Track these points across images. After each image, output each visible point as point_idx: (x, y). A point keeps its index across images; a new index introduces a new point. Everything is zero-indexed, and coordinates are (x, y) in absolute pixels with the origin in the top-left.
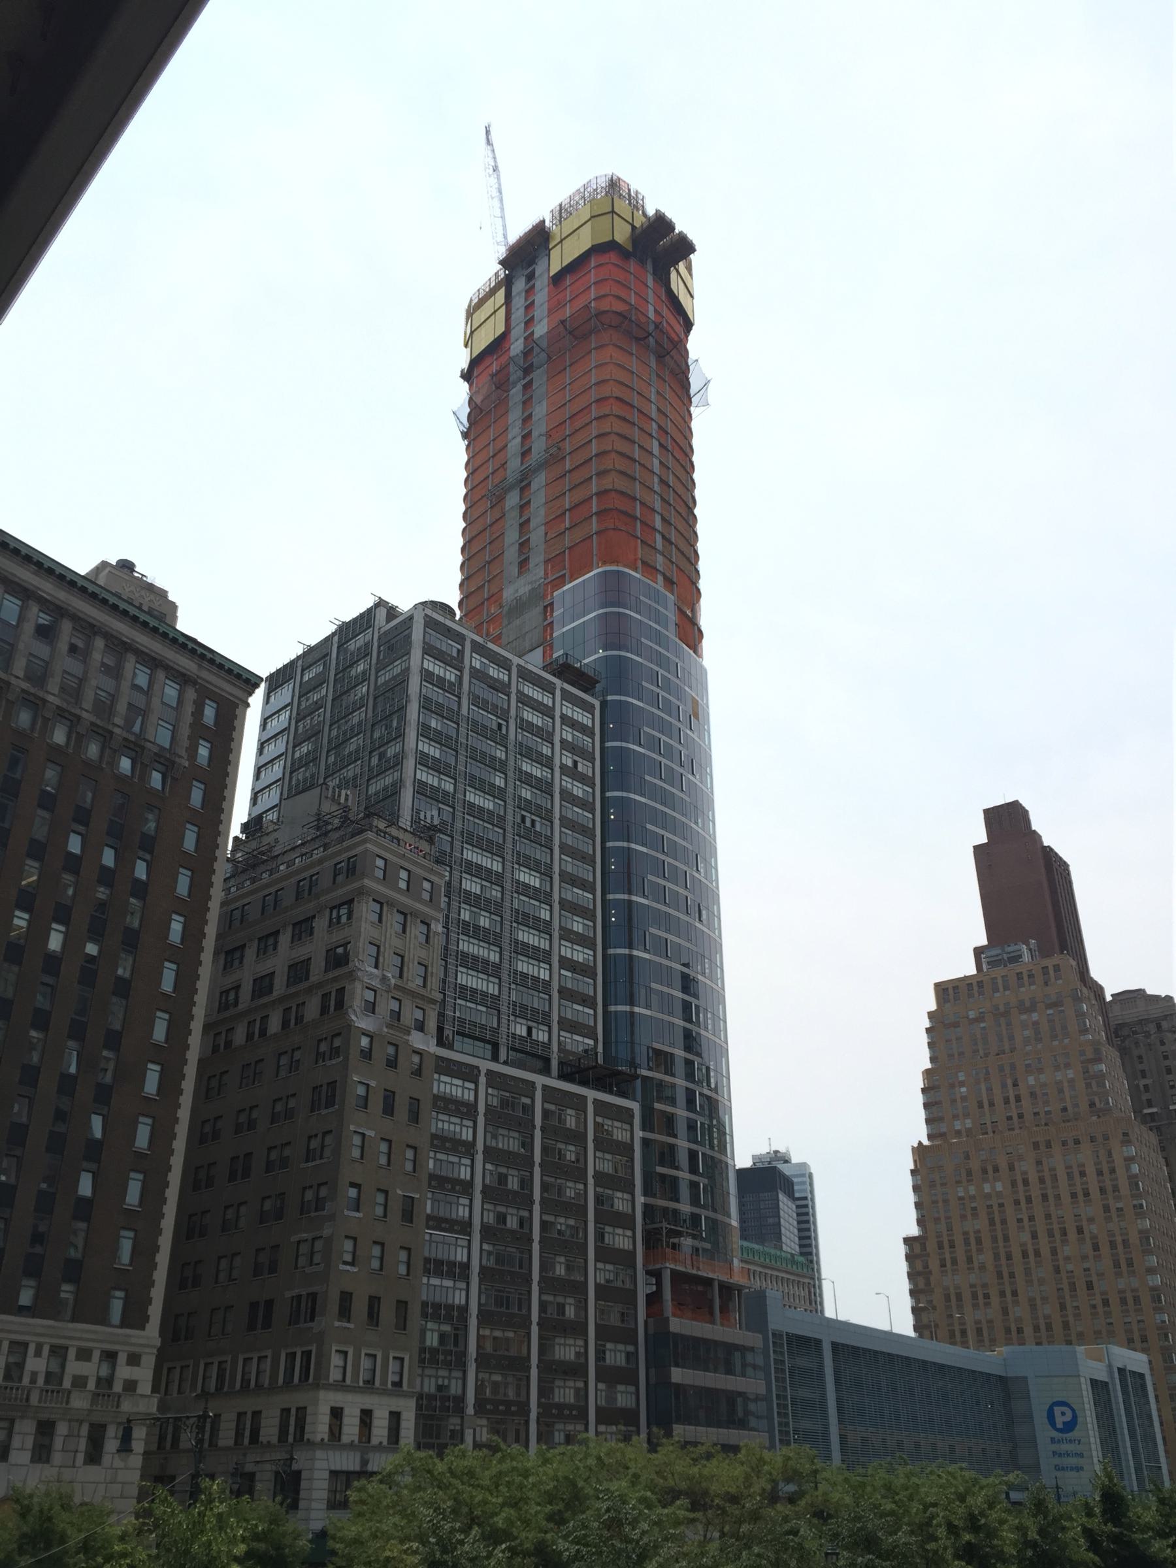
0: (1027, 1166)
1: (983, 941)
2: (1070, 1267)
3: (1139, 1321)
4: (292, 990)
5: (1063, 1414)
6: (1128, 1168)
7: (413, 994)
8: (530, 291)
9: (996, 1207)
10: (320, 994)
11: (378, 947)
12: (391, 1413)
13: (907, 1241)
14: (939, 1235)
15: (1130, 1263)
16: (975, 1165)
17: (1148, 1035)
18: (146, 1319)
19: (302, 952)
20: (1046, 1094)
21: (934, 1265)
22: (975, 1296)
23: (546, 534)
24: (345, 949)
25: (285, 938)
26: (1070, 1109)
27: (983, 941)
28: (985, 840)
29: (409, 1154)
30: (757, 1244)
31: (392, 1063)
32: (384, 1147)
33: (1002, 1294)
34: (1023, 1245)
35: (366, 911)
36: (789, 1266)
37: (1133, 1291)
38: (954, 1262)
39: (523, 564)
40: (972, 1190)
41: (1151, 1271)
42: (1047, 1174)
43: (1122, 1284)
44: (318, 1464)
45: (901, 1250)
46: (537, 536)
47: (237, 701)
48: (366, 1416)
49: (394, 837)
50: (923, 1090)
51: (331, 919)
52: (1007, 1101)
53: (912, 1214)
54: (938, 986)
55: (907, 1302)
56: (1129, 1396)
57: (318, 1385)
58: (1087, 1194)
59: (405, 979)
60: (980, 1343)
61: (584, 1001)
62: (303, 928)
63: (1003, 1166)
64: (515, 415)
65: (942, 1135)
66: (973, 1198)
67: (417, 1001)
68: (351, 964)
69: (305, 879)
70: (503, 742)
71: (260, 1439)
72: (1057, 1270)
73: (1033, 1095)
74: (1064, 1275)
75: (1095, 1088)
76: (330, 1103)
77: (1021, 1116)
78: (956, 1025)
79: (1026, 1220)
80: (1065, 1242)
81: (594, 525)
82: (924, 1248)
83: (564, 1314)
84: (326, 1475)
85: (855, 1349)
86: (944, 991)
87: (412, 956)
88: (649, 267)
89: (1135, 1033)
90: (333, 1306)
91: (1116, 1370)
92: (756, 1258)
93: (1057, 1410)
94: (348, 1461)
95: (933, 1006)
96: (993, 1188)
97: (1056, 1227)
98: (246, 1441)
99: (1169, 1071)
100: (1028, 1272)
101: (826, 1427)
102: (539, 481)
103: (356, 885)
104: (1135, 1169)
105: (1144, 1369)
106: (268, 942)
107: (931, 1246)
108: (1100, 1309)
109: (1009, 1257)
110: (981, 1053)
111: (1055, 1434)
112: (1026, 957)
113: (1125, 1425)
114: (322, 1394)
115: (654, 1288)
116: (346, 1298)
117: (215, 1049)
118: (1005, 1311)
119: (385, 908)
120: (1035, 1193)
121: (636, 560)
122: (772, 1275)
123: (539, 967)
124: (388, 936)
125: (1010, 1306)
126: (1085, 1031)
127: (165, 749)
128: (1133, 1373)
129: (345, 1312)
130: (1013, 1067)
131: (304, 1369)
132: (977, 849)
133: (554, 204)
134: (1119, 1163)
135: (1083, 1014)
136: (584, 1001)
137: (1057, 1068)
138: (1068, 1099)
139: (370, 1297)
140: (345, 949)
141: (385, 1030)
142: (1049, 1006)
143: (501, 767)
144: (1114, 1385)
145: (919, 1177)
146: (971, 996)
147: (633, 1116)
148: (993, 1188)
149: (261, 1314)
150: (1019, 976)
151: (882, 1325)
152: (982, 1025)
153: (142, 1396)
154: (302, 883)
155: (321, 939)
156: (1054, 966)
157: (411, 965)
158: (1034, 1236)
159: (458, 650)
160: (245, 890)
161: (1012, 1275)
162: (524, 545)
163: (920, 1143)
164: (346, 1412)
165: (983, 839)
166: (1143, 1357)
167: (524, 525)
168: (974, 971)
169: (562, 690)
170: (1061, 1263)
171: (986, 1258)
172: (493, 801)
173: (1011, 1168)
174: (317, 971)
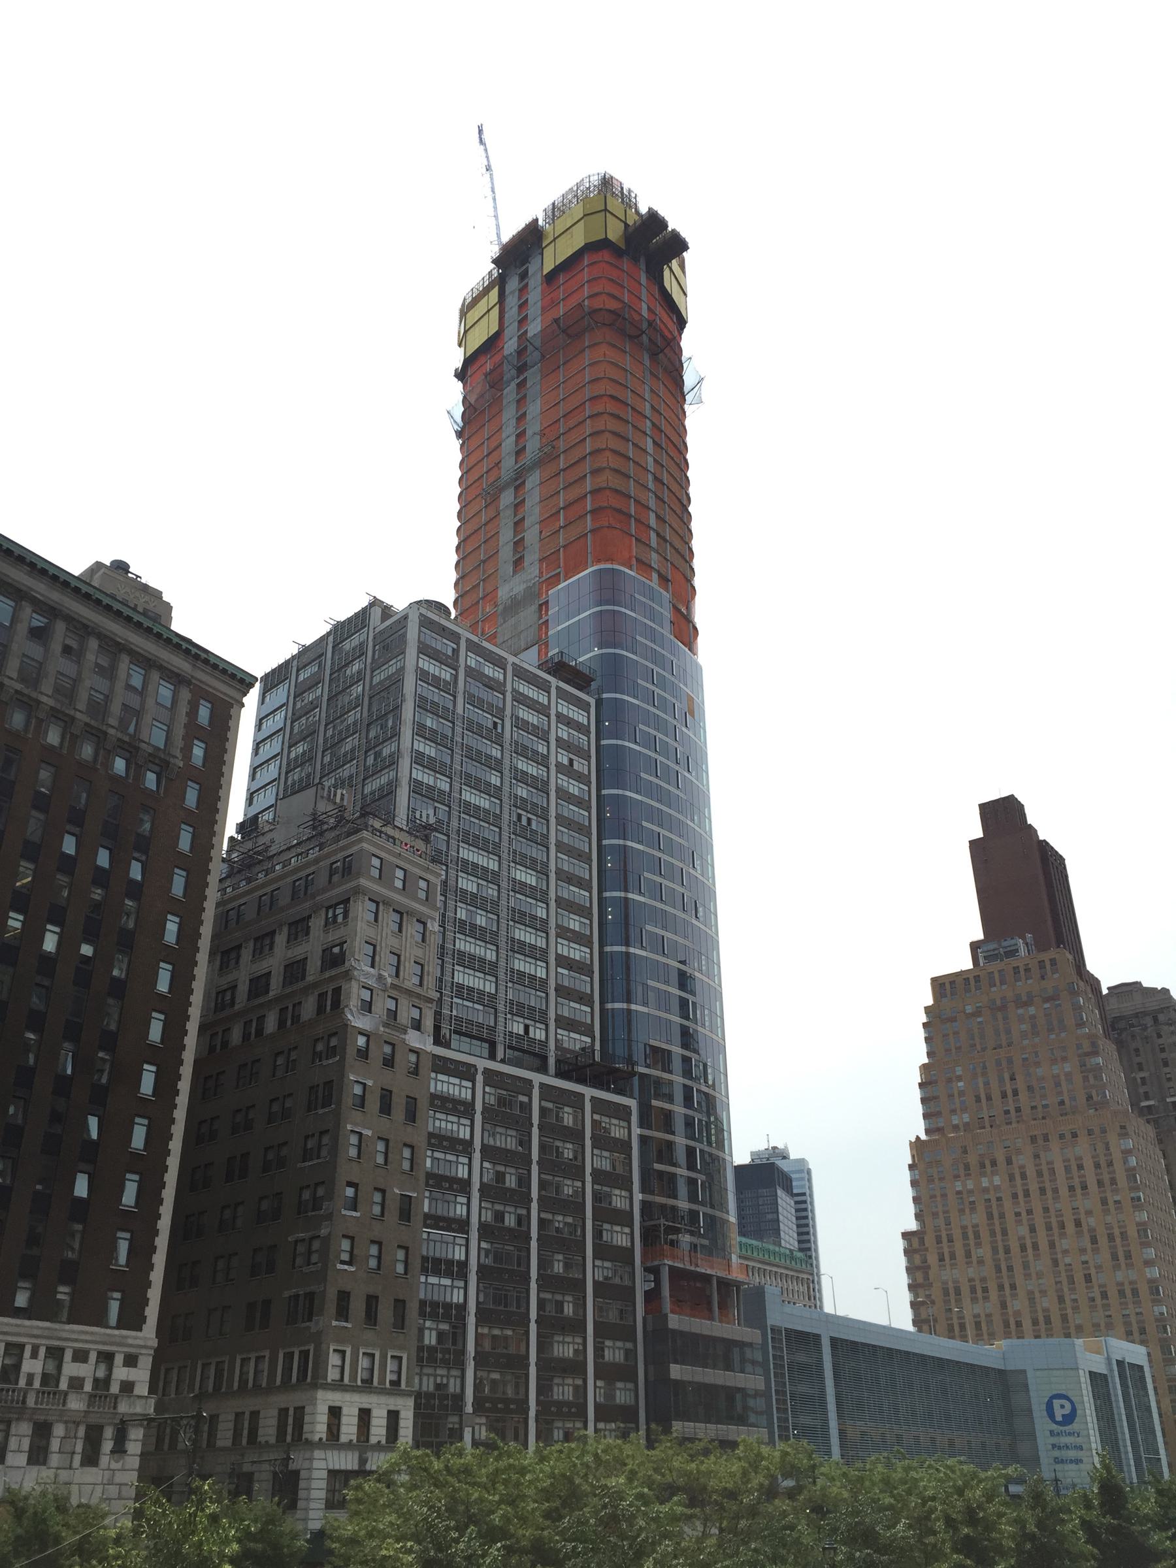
0: (1024, 1159)
1: (980, 936)
2: (1068, 1260)
3: (1137, 1314)
4: (288, 990)
5: (1062, 1407)
6: (1125, 1162)
7: (409, 993)
8: (523, 290)
9: (994, 1203)
11: (375, 946)
14: (937, 1230)
15: (1128, 1256)
21: (932, 1259)
22: (973, 1290)
23: (541, 532)
24: (341, 949)
25: (281, 939)
26: (1067, 1101)
28: (981, 835)
29: (407, 1153)
32: (381, 1146)
33: (1001, 1287)
34: (1021, 1238)
35: (362, 910)
37: (1131, 1283)
38: (953, 1256)
39: (518, 563)
40: (970, 1185)
43: (1120, 1276)
44: (316, 1464)
45: (900, 1244)
46: (531, 535)
48: (365, 1415)
49: (389, 836)
50: (920, 1085)
51: (327, 918)
52: (1004, 1095)
53: (910, 1209)
54: (934, 981)
58: (1084, 1187)
59: (401, 978)
60: (979, 1337)
61: (581, 999)
62: (299, 929)
63: (1000, 1157)
64: (509, 414)
65: (939, 1130)
66: (970, 1192)
68: (347, 964)
70: (499, 741)
72: (1055, 1263)
74: (1062, 1267)
77: (1018, 1110)
80: (1063, 1235)
83: (562, 1311)
87: (407, 954)
88: (643, 266)
89: (1132, 1026)
91: (1114, 1362)
94: (346, 1461)
95: (930, 1001)
96: (991, 1182)
100: (1026, 1266)
101: (826, 1421)
102: (533, 480)
104: (1133, 1161)
105: (1142, 1360)
106: (263, 943)
107: (930, 1240)
108: (1099, 1301)
109: (1007, 1251)
110: (979, 1047)
111: (1054, 1427)
112: (1023, 951)
114: (321, 1394)
116: (344, 1297)
117: (212, 1049)
118: (1004, 1305)
119: (381, 907)
120: (1034, 1187)
121: (630, 558)
124: (384, 935)
125: (1008, 1299)
126: (1081, 1024)
130: (1010, 1061)
132: (973, 844)
133: (547, 203)
134: (1117, 1156)
135: (1080, 1007)
136: (581, 999)
137: (1054, 1061)
140: (341, 949)
141: (382, 1029)
142: (1047, 1000)
144: (1113, 1377)
145: (917, 1172)
146: (968, 990)
147: (630, 1114)
148: (991, 1182)
150: (1016, 970)
153: (139, 1397)
154: (334, 866)
156: (1051, 960)
158: (1033, 1230)
160: (240, 891)
161: (1010, 1268)
162: (519, 544)
163: (918, 1138)
165: (979, 833)
166: (1142, 1350)
167: (518, 524)
169: (558, 688)
171: (985, 1252)
173: (1009, 1162)
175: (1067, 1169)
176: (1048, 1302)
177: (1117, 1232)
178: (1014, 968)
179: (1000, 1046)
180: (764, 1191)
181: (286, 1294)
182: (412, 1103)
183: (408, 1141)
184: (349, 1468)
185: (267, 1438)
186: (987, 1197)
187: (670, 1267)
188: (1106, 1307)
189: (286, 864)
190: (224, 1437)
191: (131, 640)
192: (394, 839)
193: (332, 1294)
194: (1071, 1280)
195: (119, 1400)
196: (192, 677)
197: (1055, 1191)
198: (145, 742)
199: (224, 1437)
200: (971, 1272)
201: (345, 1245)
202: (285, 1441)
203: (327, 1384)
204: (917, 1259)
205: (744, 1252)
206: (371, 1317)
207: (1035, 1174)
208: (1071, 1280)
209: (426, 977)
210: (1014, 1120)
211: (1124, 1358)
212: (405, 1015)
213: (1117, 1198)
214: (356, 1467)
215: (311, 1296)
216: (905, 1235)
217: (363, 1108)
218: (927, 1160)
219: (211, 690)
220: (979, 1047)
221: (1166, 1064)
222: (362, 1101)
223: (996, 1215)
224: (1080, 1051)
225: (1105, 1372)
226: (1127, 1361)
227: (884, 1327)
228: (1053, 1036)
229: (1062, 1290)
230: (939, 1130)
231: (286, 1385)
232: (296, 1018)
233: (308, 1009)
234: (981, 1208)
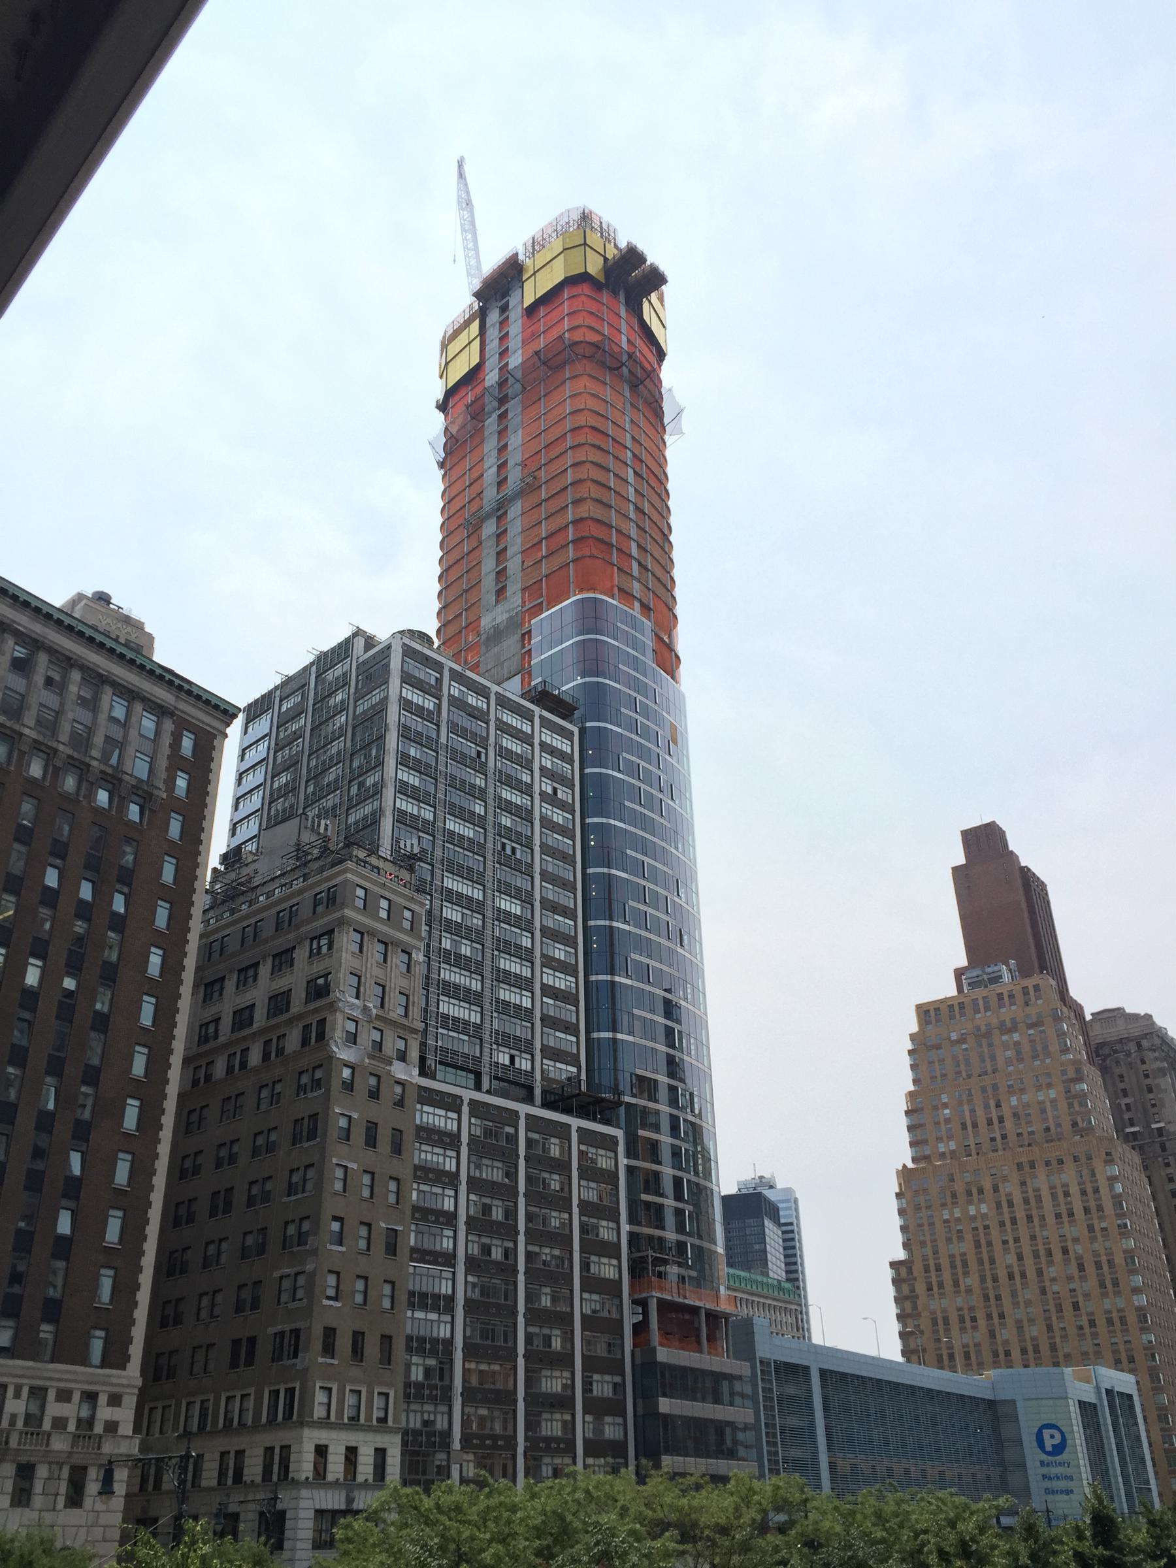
0: (1011, 1188)
2: (1056, 1288)
3: (1126, 1342)
4: (273, 1022)
5: (1052, 1437)
6: (1111, 1187)
7: (394, 1024)
8: (503, 323)
9: (981, 1229)
11: (359, 977)
13: (894, 1265)
14: (925, 1259)
15: (1116, 1284)
16: (959, 1187)
17: (1128, 1054)
19: (281, 984)
20: (1029, 1114)
21: (921, 1288)
22: (962, 1320)
24: (326, 980)
25: (265, 970)
26: (1052, 1128)
27: (963, 962)
29: (393, 1186)
33: (989, 1317)
34: (1009, 1267)
37: (1118, 1311)
38: (941, 1285)
39: (501, 592)
40: (957, 1213)
41: (1136, 1291)
42: (1031, 1194)
43: (1107, 1304)
45: (889, 1274)
47: (214, 732)
48: (351, 1453)
51: (311, 950)
52: (990, 1122)
53: (898, 1238)
54: (919, 1007)
60: (968, 1367)
62: (283, 959)
63: (987, 1184)
64: (491, 445)
65: (926, 1158)
66: (958, 1220)
70: (482, 770)
71: (245, 1478)
72: (1043, 1291)
73: (1016, 1115)
74: (1050, 1296)
75: (1077, 1108)
76: (312, 1135)
77: (1004, 1137)
79: (1011, 1241)
80: (1050, 1263)
81: (571, 553)
82: (910, 1271)
85: (843, 1375)
86: (927, 1013)
87: (393, 985)
89: (1115, 1052)
90: (317, 1344)
93: (1046, 1433)
94: (334, 1500)
95: (915, 1028)
96: (978, 1210)
97: (1041, 1248)
99: (1150, 1090)
100: (1014, 1294)
102: (515, 510)
103: (338, 915)
104: (1119, 1188)
105: (1132, 1390)
107: (918, 1269)
108: (1087, 1330)
109: (995, 1279)
110: (964, 1074)
111: (1044, 1457)
112: (1006, 977)
114: (307, 1432)
115: (641, 1317)
116: (330, 1333)
117: (195, 1083)
120: (1020, 1215)
123: (522, 995)
124: (369, 966)
126: (1066, 1050)
127: (143, 781)
130: (995, 1087)
131: (287, 1407)
132: (956, 870)
133: (527, 237)
137: (1039, 1088)
138: (1051, 1119)
140: (326, 980)
143: (481, 794)
144: (1102, 1405)
145: (904, 1201)
146: (952, 1017)
147: (616, 1144)
150: (1000, 996)
151: (866, 1348)
152: (964, 1046)
158: (1020, 1257)
160: (223, 922)
161: (998, 1298)
162: (501, 574)
163: (904, 1166)
164: (331, 1449)
165: (961, 860)
166: (1130, 1379)
167: (501, 554)
169: (541, 717)
170: (1047, 1284)
171: (973, 1281)
173: (996, 1189)
175: (1054, 1196)
176: (1036, 1330)
178: (998, 994)
179: (986, 1073)
181: (271, 1331)
183: (395, 1175)
186: (973, 1225)
187: (659, 1299)
188: (1095, 1335)
192: (378, 869)
193: (317, 1332)
194: (1060, 1309)
196: (175, 708)
197: (1043, 1218)
200: (959, 1301)
204: (905, 1289)
206: (357, 1352)
208: (1060, 1309)
209: (411, 1008)
210: (1000, 1147)
211: (1113, 1387)
212: (390, 1045)
213: (1103, 1225)
216: (894, 1265)
220: (964, 1074)
221: (1150, 1090)
223: (983, 1241)
224: (1065, 1078)
225: (1094, 1401)
227: (873, 1358)
228: (1037, 1063)
229: (1050, 1318)
230: (926, 1158)
232: (280, 1051)
233: (293, 1042)
234: (968, 1237)
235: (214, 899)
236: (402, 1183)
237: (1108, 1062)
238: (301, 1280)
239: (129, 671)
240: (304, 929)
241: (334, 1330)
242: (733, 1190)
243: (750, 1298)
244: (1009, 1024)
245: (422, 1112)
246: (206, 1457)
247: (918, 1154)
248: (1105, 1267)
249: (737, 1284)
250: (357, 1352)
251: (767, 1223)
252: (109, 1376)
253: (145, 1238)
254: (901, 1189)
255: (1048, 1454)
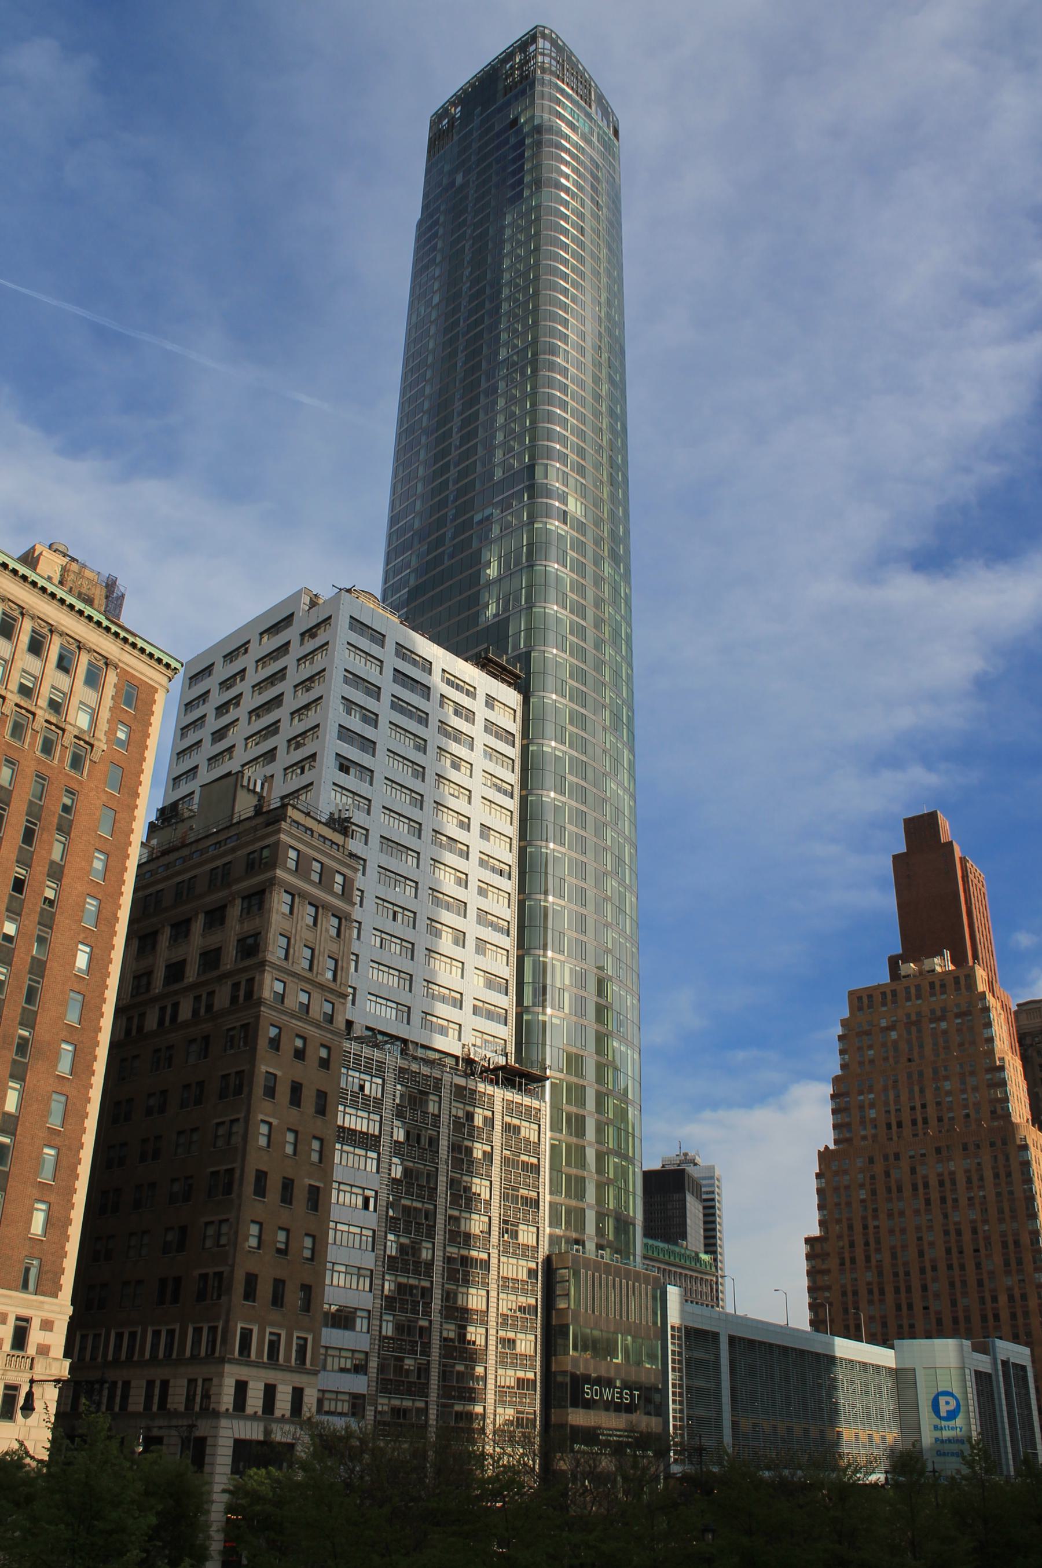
4: (203, 978)
5: (947, 1403)
7: (321, 987)
10: (229, 983)
11: (289, 939)
12: (294, 1389)
13: (808, 1241)
18: (60, 1288)
19: (214, 940)
24: (256, 941)
25: (198, 926)
29: (316, 1145)
30: (661, 1241)
31: (300, 1054)
32: (290, 1137)
35: (280, 902)
36: (693, 1264)
38: (853, 1260)
44: (223, 1432)
45: (803, 1249)
47: (156, 686)
48: (270, 1391)
49: (307, 829)
53: (815, 1216)
55: (804, 1299)
56: (1010, 1386)
57: (224, 1358)
59: (315, 972)
62: (216, 917)
65: (848, 1141)
67: (326, 994)
68: (261, 955)
69: (255, 851)
71: (168, 1406)
76: (239, 1090)
78: (868, 1033)
84: (231, 1443)
85: (751, 1342)
86: (860, 1000)
87: (322, 949)
90: (239, 1287)
91: (999, 1362)
92: (661, 1256)
93: (942, 1400)
94: (253, 1431)
98: (155, 1408)
101: (719, 1412)
103: (269, 875)
105: (1027, 1362)
106: (181, 929)
111: (937, 1421)
113: (1005, 1414)
114: (228, 1368)
116: (251, 1280)
117: (128, 1032)
119: (297, 900)
120: (935, 1196)
122: (675, 1272)
124: (299, 928)
127: (85, 731)
128: (1015, 1365)
129: (250, 1294)
131: (210, 1344)
139: (275, 1280)
140: (256, 941)
142: (958, 1016)
144: (997, 1376)
145: (823, 1180)
149: (119, 1392)
151: (777, 1318)
153: (54, 1359)
154: (252, 856)
155: (235, 926)
156: (892, 991)
157: (321, 958)
159: (484, 1152)
160: (159, 876)
163: (827, 1147)
164: (251, 1385)
166: (1027, 1351)
168: (887, 979)
172: (410, 795)
174: (230, 959)
177: (1010, 1240)
178: (858, 998)
180: (676, 1196)
181: (197, 1273)
182: (322, 1096)
183: (318, 1134)
184: (254, 1437)
185: (175, 1406)
189: (202, 852)
190: (137, 1402)
191: (62, 622)
192: (312, 831)
193: (239, 1277)
195: (35, 1361)
196: (119, 660)
198: (71, 724)
199: (137, 1402)
201: (254, 1229)
202: (193, 1409)
203: (234, 1359)
205: (650, 1253)
206: (277, 1300)
207: (937, 1183)
209: (339, 973)
211: (1009, 1358)
212: (317, 1008)
214: (261, 1438)
215: (219, 1275)
216: (808, 1241)
217: (274, 1098)
218: (834, 1168)
219: (137, 674)
222: (270, 1092)
225: (989, 1371)
226: (1011, 1361)
227: (781, 1327)
231: (194, 1358)
233: (222, 998)
235: (151, 853)
236: (325, 1143)
237: (1030, 1051)
238: (225, 1229)
239: (78, 622)
240: (235, 888)
241: (256, 1276)
242: (656, 1166)
243: (666, 1267)
244: (939, 1013)
245: (345, 1113)
246: (133, 1384)
247: (841, 1136)
248: (1011, 1247)
249: (655, 1254)
250: (277, 1300)
251: (690, 1199)
252: (42, 1302)
253: (77, 1177)
254: (820, 1169)
255: (940, 1418)
